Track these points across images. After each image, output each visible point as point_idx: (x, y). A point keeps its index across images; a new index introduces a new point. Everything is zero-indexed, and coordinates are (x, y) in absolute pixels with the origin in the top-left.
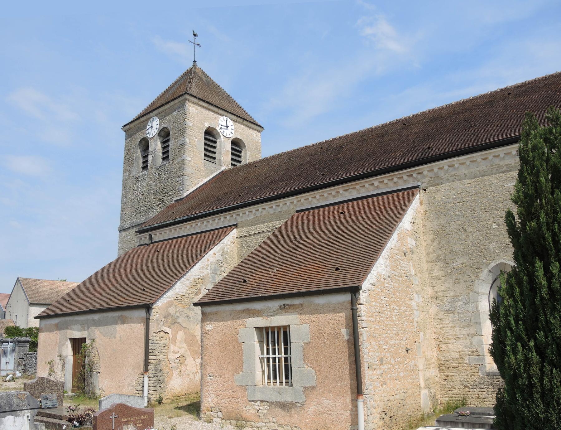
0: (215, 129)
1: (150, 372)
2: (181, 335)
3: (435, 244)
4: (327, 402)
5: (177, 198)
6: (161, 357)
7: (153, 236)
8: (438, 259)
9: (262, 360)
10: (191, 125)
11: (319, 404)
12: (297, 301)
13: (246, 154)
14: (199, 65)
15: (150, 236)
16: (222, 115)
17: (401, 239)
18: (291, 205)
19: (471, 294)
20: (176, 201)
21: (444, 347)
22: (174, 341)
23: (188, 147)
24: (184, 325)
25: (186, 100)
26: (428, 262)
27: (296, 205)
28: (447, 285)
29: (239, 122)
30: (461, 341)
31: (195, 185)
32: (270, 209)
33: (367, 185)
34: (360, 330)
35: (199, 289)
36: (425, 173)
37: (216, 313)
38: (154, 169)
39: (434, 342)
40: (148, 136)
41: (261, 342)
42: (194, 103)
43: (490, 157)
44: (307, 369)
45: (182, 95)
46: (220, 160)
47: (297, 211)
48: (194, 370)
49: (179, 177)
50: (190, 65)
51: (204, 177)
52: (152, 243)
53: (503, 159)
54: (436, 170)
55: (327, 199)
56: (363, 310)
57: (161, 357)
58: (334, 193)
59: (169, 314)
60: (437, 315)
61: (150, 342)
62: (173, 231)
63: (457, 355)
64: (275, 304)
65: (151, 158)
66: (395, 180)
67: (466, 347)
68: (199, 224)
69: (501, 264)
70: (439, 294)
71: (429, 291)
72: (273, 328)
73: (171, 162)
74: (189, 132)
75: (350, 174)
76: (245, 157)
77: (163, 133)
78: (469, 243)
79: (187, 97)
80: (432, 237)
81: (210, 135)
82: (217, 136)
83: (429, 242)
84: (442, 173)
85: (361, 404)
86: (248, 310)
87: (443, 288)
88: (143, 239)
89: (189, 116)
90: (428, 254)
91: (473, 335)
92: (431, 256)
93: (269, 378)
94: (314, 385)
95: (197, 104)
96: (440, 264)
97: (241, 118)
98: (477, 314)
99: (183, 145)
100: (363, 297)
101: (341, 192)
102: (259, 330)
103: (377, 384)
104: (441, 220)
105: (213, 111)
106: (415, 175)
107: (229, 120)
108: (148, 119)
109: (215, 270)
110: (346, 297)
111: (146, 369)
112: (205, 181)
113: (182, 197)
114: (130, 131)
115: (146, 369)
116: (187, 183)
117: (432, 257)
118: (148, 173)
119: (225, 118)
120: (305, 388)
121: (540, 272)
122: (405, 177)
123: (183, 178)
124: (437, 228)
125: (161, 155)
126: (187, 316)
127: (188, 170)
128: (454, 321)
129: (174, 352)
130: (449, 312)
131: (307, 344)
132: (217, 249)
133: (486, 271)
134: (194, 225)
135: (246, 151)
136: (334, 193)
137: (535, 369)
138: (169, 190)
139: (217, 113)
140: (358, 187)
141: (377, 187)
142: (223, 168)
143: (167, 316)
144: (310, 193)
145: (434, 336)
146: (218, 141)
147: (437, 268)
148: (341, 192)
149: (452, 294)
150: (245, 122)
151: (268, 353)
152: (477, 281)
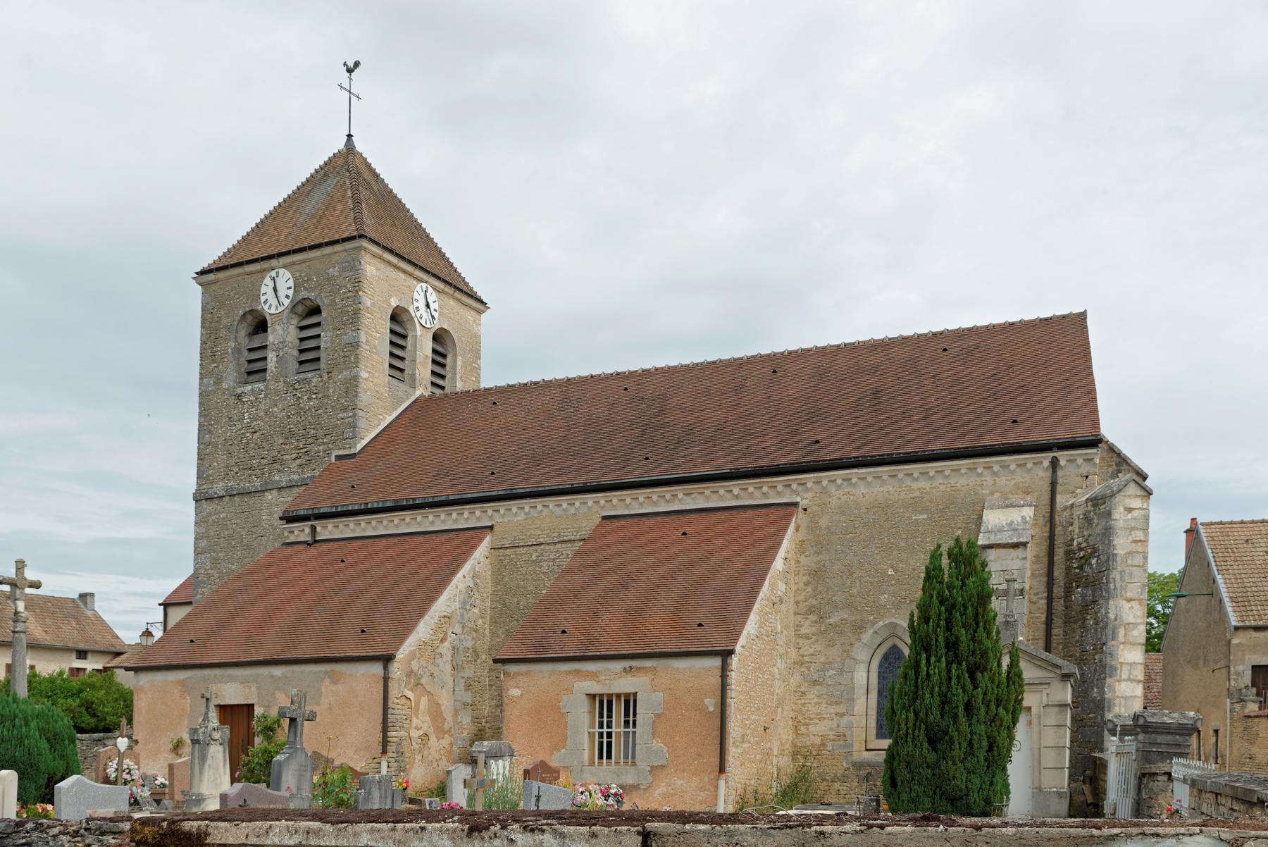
0: (407, 311)
1: (390, 754)
2: (424, 702)
3: (809, 589)
4: (679, 782)
5: (341, 453)
6: (403, 733)
7: (318, 529)
8: (811, 610)
9: (591, 735)
10: (368, 303)
11: (668, 785)
12: (648, 663)
13: (455, 361)
14: (360, 146)
15: (313, 529)
16: (421, 281)
17: (773, 587)
18: (592, 508)
19: (848, 661)
20: (338, 458)
21: (803, 729)
22: (416, 711)
23: (364, 350)
24: (428, 688)
25: (360, 248)
26: (796, 613)
27: (602, 508)
28: (818, 647)
29: (447, 293)
30: (826, 722)
31: (374, 427)
32: (557, 509)
33: (722, 492)
34: (729, 700)
35: (446, 633)
36: (809, 485)
37: (527, 673)
38: (281, 384)
39: (790, 723)
40: (266, 308)
41: (592, 712)
42: (374, 256)
43: (901, 476)
44: (657, 744)
45: (353, 238)
46: (414, 375)
47: (604, 518)
48: (437, 756)
49: (345, 409)
50: (340, 145)
51: (388, 410)
52: (316, 541)
53: (916, 480)
54: (825, 483)
55: (655, 503)
56: (734, 677)
57: (403, 733)
58: (668, 496)
59: (412, 672)
60: (799, 686)
61: (390, 711)
62: (363, 524)
63: (818, 740)
64: (618, 666)
65: (275, 359)
66: (765, 489)
67: (831, 729)
68: (419, 518)
69: (891, 623)
70: (806, 659)
71: (793, 655)
72: (610, 695)
73: (325, 377)
74: (366, 319)
75: (696, 469)
76: (454, 368)
77: (300, 309)
78: (855, 591)
79: (365, 243)
80: (806, 578)
81: (398, 317)
82: (408, 326)
83: (801, 586)
84: (832, 488)
85: (722, 783)
86: (577, 672)
87: (812, 651)
88: (296, 532)
89: (365, 284)
90: (797, 603)
91: (842, 715)
92: (801, 605)
93: (601, 757)
94: (664, 763)
95: (381, 258)
96: (813, 617)
97: (450, 285)
98: (851, 689)
99: (355, 345)
100: (734, 661)
101: (680, 496)
102: (592, 697)
103: (738, 763)
104: (822, 556)
105: (405, 272)
106: (794, 486)
107: (430, 290)
108: (264, 271)
109: (464, 603)
110: (717, 662)
111: (384, 752)
112: (389, 419)
113: (352, 451)
114: (214, 287)
115: (384, 752)
116: (362, 424)
117: (803, 607)
118: (267, 387)
119: (424, 285)
120: (652, 767)
121: (924, 662)
122: (780, 488)
123: (355, 415)
124: (814, 567)
125: (296, 353)
126: (432, 674)
127: (364, 398)
128: (819, 696)
129: (417, 729)
130: (815, 683)
131: (658, 716)
132: (466, 569)
133: (870, 632)
134: (408, 520)
135: (455, 356)
136: (668, 496)
137: (910, 725)
138: (321, 432)
139: (411, 275)
140: (707, 492)
141: (737, 497)
142: (418, 393)
143: (410, 673)
144: (629, 492)
145: (792, 714)
146: (410, 334)
147: (808, 623)
148: (680, 496)
149: (822, 659)
150: (458, 295)
151: (601, 726)
152: (858, 644)
